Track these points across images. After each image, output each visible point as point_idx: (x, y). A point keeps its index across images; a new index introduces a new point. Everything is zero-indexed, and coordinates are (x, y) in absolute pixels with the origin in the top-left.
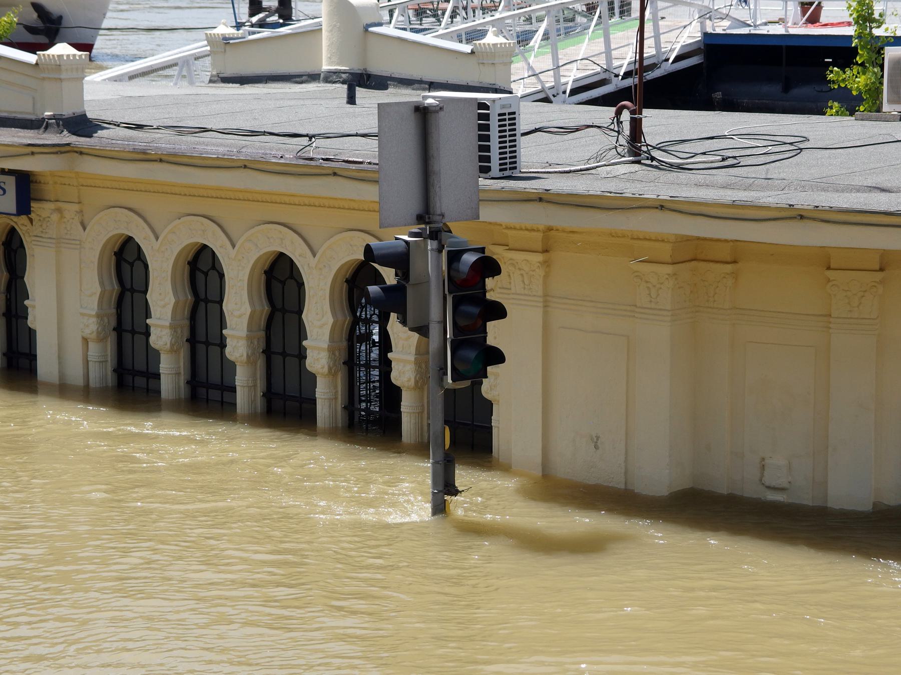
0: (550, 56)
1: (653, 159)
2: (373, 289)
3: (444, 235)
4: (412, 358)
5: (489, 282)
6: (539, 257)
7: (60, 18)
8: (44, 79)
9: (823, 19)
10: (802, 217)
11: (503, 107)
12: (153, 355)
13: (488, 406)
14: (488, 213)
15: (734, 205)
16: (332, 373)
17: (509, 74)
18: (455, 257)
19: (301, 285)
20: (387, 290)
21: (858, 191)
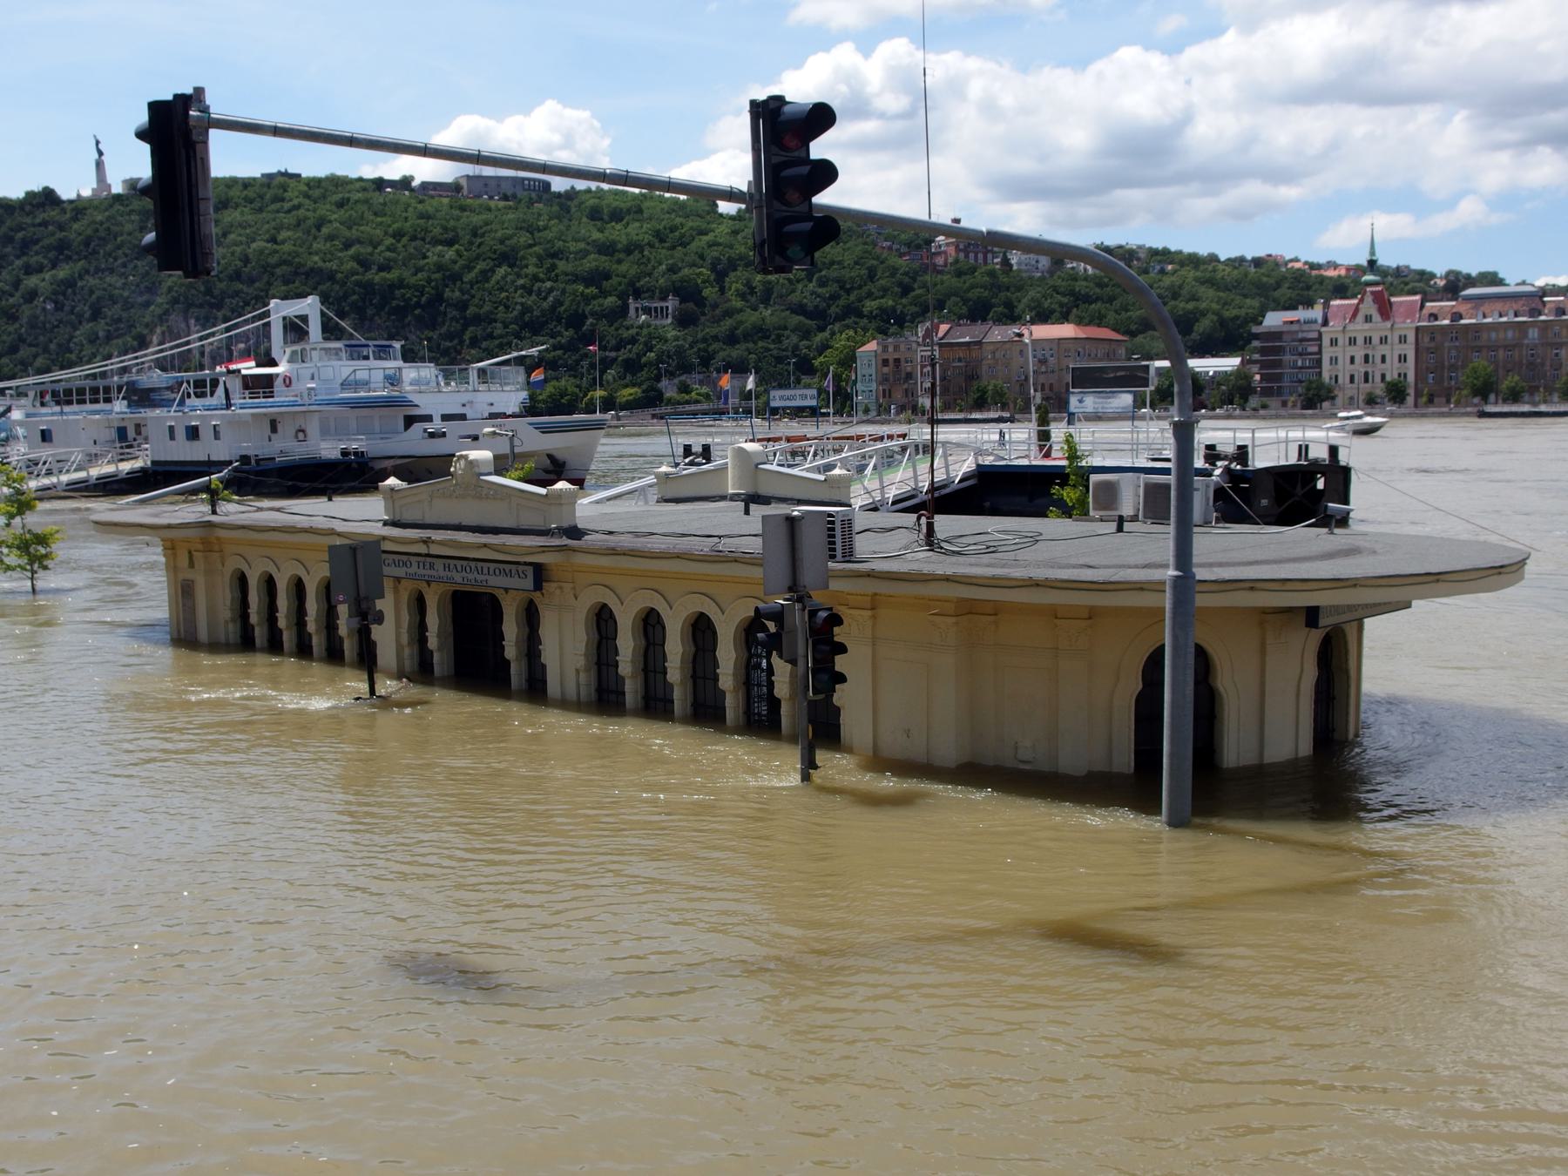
0: (878, 481)
1: (942, 548)
2: (760, 635)
3: (806, 599)
4: (787, 680)
5: (836, 630)
6: (869, 613)
7: (565, 463)
8: (551, 504)
9: (1054, 454)
10: (1038, 585)
11: (844, 516)
12: (620, 680)
13: (838, 710)
14: (835, 585)
15: (994, 578)
16: (736, 690)
17: (849, 493)
18: (813, 614)
19: (715, 633)
20: (770, 636)
21: (1074, 567)
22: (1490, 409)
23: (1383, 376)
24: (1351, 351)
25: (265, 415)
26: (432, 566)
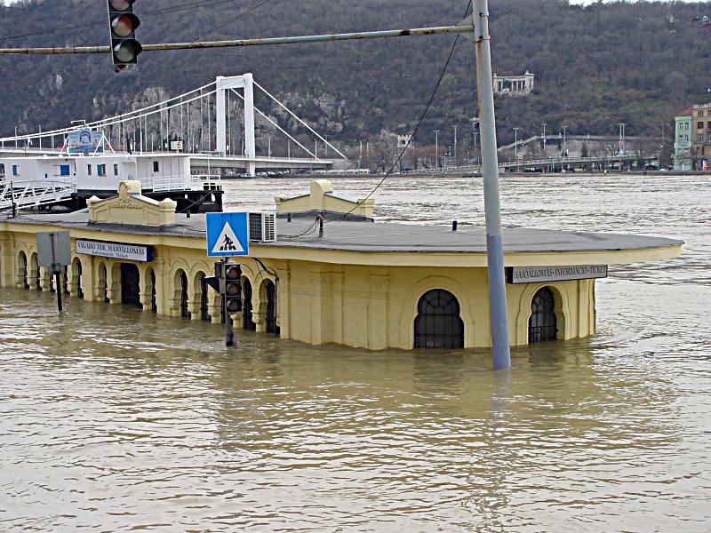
25: (150, 158)
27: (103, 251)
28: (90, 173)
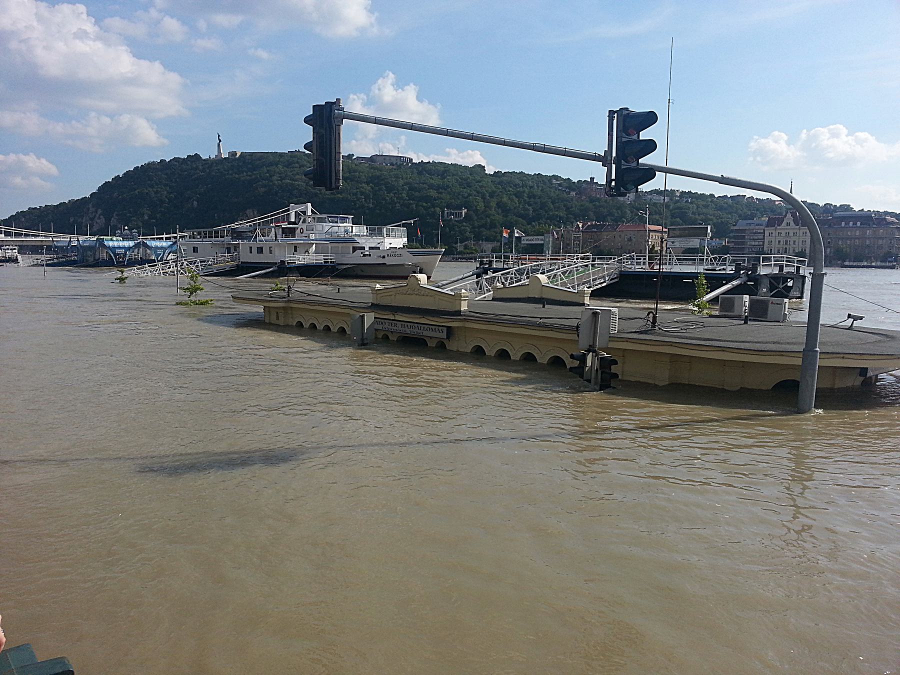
22: (847, 263)
23: (794, 250)
24: (779, 239)
26: (395, 325)
27: (396, 328)
28: (251, 252)
